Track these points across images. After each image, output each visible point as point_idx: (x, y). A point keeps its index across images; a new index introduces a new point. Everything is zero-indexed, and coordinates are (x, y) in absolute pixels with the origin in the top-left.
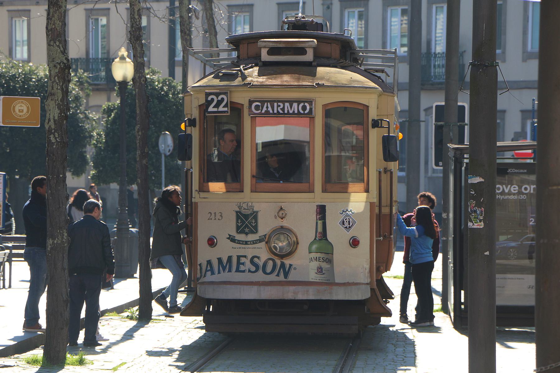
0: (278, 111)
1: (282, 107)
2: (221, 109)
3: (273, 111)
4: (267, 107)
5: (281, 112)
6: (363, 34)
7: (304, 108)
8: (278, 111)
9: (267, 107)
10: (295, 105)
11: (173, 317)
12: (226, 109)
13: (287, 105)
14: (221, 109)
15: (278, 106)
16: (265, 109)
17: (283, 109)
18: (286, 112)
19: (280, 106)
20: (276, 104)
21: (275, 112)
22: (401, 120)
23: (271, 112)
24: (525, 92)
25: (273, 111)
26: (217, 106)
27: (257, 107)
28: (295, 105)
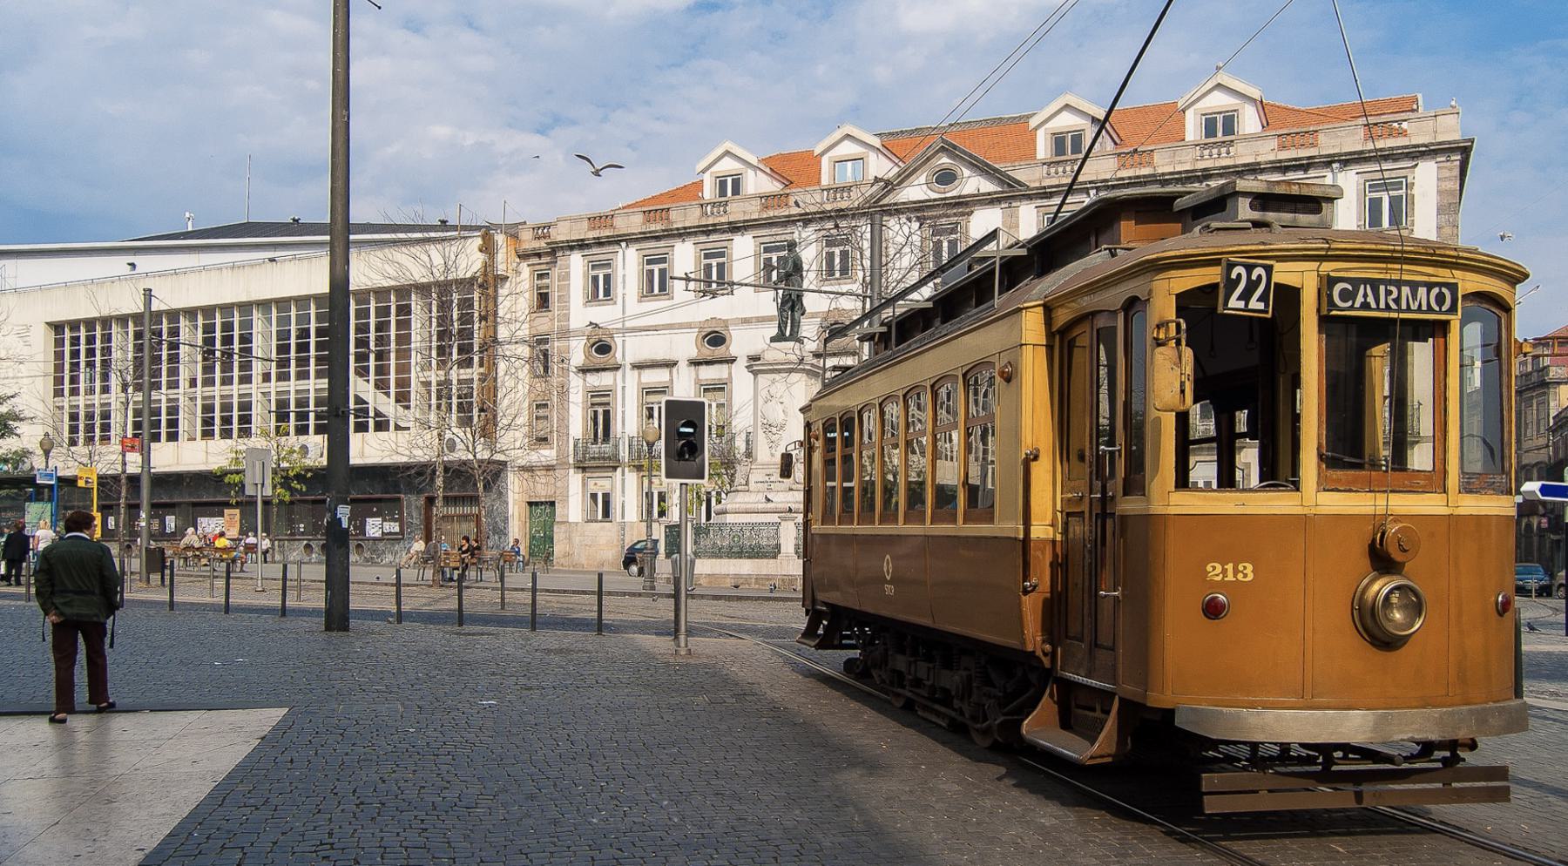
0: (1387, 304)
1: (1395, 295)
2: (1255, 304)
3: (1377, 303)
4: (1365, 295)
5: (1393, 306)
6: (800, 588)
7: (1440, 299)
8: (1387, 304)
9: (1365, 295)
10: (1422, 291)
11: (63, 721)
12: (1261, 306)
13: (1406, 290)
14: (1255, 304)
15: (1389, 293)
16: (1360, 300)
17: (1397, 301)
18: (1404, 306)
19: (1391, 293)
20: (1382, 288)
21: (1382, 305)
22: (1535, 475)
23: (1373, 305)
24: (767, 324)
25: (1377, 303)
26: (1245, 296)
27: (1345, 295)
28: (1422, 291)
